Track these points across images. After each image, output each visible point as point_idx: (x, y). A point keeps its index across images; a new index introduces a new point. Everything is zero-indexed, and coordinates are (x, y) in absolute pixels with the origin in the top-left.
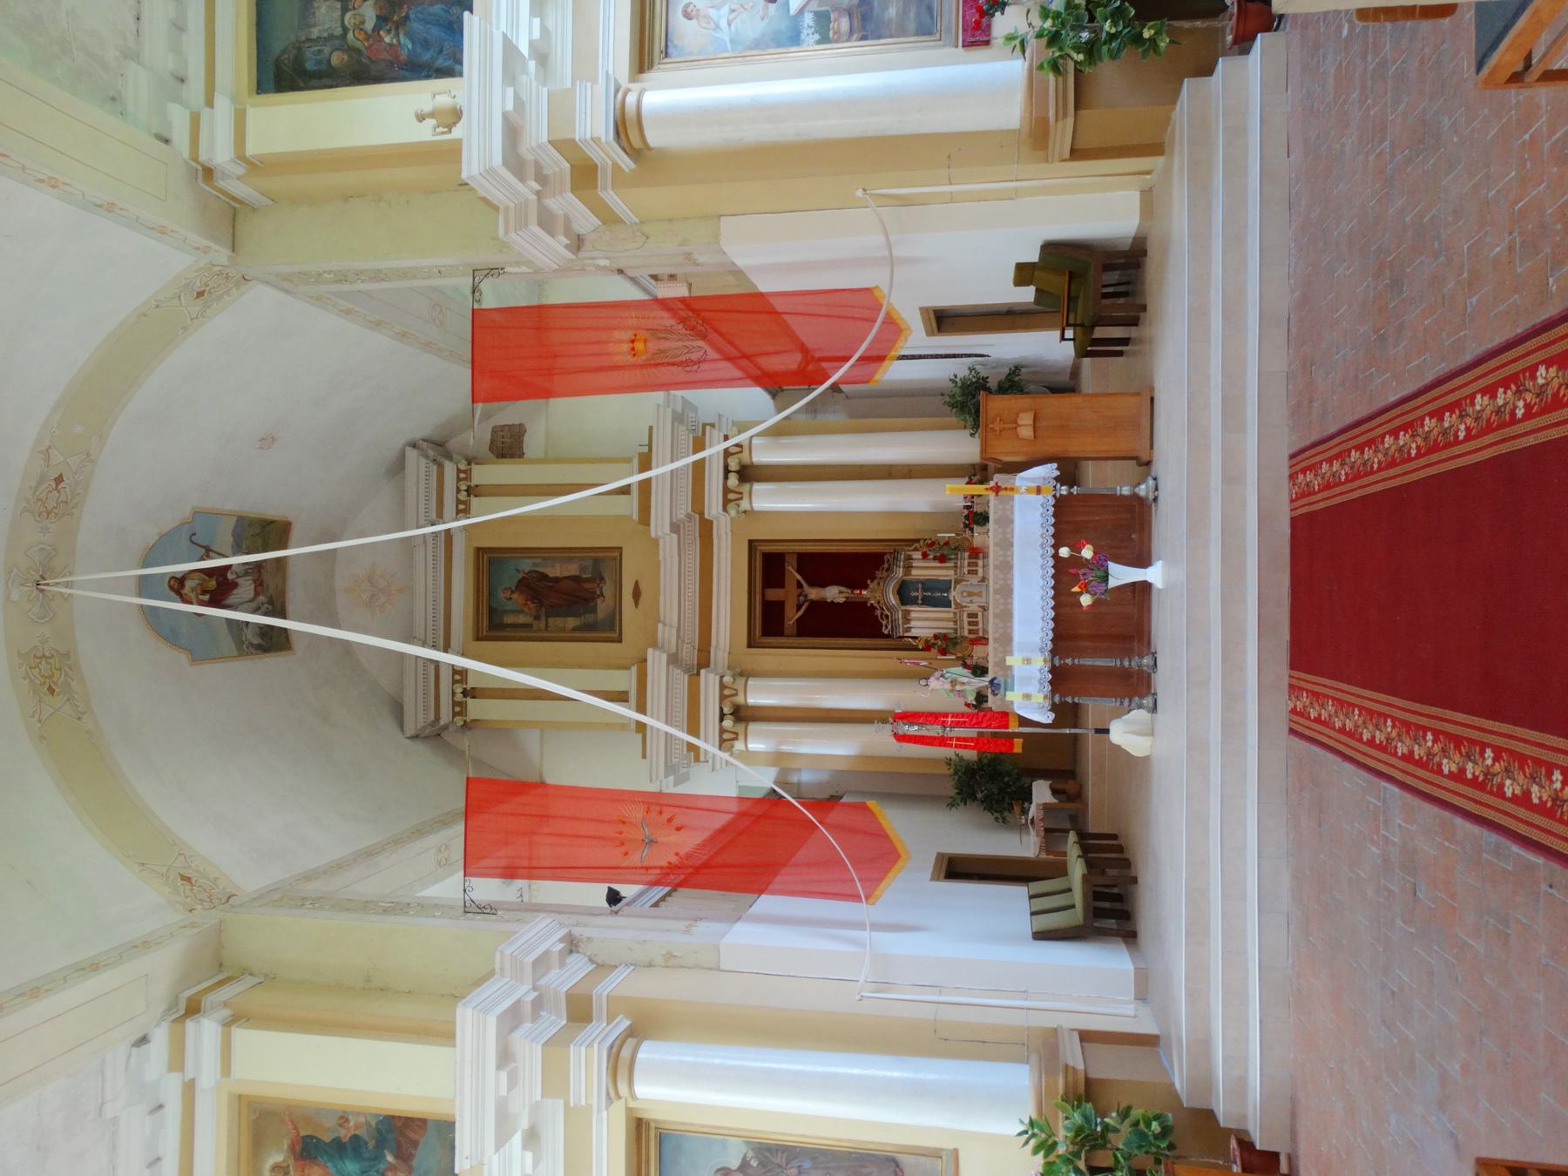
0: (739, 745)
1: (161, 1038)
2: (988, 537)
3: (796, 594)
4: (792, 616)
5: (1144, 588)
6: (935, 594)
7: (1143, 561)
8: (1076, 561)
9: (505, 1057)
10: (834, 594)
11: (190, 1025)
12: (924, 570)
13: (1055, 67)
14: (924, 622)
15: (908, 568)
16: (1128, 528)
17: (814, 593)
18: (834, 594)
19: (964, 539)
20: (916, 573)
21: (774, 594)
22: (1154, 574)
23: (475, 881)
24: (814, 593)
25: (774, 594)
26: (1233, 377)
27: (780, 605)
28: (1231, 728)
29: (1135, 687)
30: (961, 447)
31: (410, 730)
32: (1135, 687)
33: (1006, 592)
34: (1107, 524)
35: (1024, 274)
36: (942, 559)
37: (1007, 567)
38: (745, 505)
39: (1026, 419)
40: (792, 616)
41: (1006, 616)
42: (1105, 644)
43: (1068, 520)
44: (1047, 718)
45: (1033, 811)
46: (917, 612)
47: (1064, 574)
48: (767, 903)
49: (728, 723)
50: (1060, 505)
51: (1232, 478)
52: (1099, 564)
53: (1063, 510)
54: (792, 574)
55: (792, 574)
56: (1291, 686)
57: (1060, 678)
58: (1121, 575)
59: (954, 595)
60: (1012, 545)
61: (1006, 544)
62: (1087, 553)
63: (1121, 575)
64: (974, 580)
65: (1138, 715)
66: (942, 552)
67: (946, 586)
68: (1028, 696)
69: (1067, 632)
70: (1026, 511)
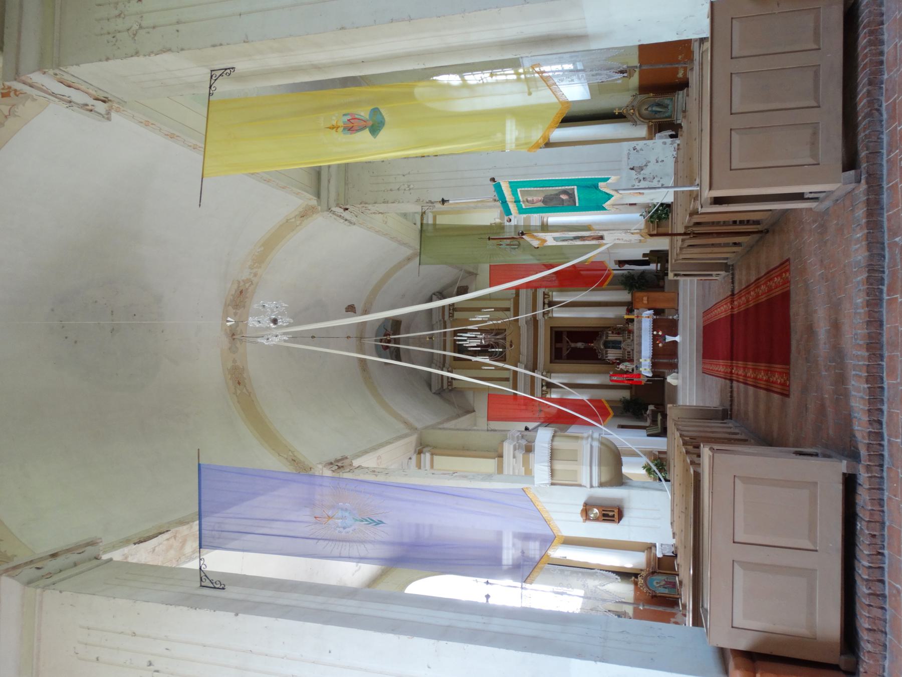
0: (548, 396)
1: (414, 457)
2: (634, 326)
3: (568, 345)
4: (565, 353)
5: (675, 342)
6: (616, 345)
7: (675, 335)
8: (658, 335)
9: (514, 457)
10: (580, 345)
11: (422, 455)
12: (612, 337)
13: (652, 222)
14: (612, 354)
15: (607, 336)
16: (672, 327)
17: (573, 345)
18: (580, 345)
19: (625, 328)
20: (610, 338)
21: (559, 345)
22: (677, 339)
23: (491, 423)
24: (573, 345)
25: (559, 345)
26: (692, 294)
27: (561, 349)
28: (691, 373)
29: (674, 367)
30: (624, 296)
31: (434, 391)
32: (674, 367)
33: (640, 344)
34: (665, 324)
35: (644, 255)
36: (619, 334)
37: (640, 336)
38: (550, 315)
39: (645, 299)
40: (565, 353)
41: (640, 352)
42: (665, 357)
43: (656, 325)
44: (650, 375)
45: (648, 412)
46: (610, 351)
47: (655, 338)
48: (573, 426)
49: (544, 388)
50: (654, 321)
51: (691, 318)
52: (663, 337)
53: (655, 322)
54: (565, 338)
55: (565, 338)
56: (317, 173)
57: (654, 365)
58: (669, 339)
59: (622, 345)
60: (345, 87)
61: (640, 329)
62: (660, 333)
63: (669, 339)
64: (629, 341)
65: (674, 374)
66: (619, 331)
67: (620, 342)
68: (646, 370)
69: (656, 353)
70: (646, 321)
